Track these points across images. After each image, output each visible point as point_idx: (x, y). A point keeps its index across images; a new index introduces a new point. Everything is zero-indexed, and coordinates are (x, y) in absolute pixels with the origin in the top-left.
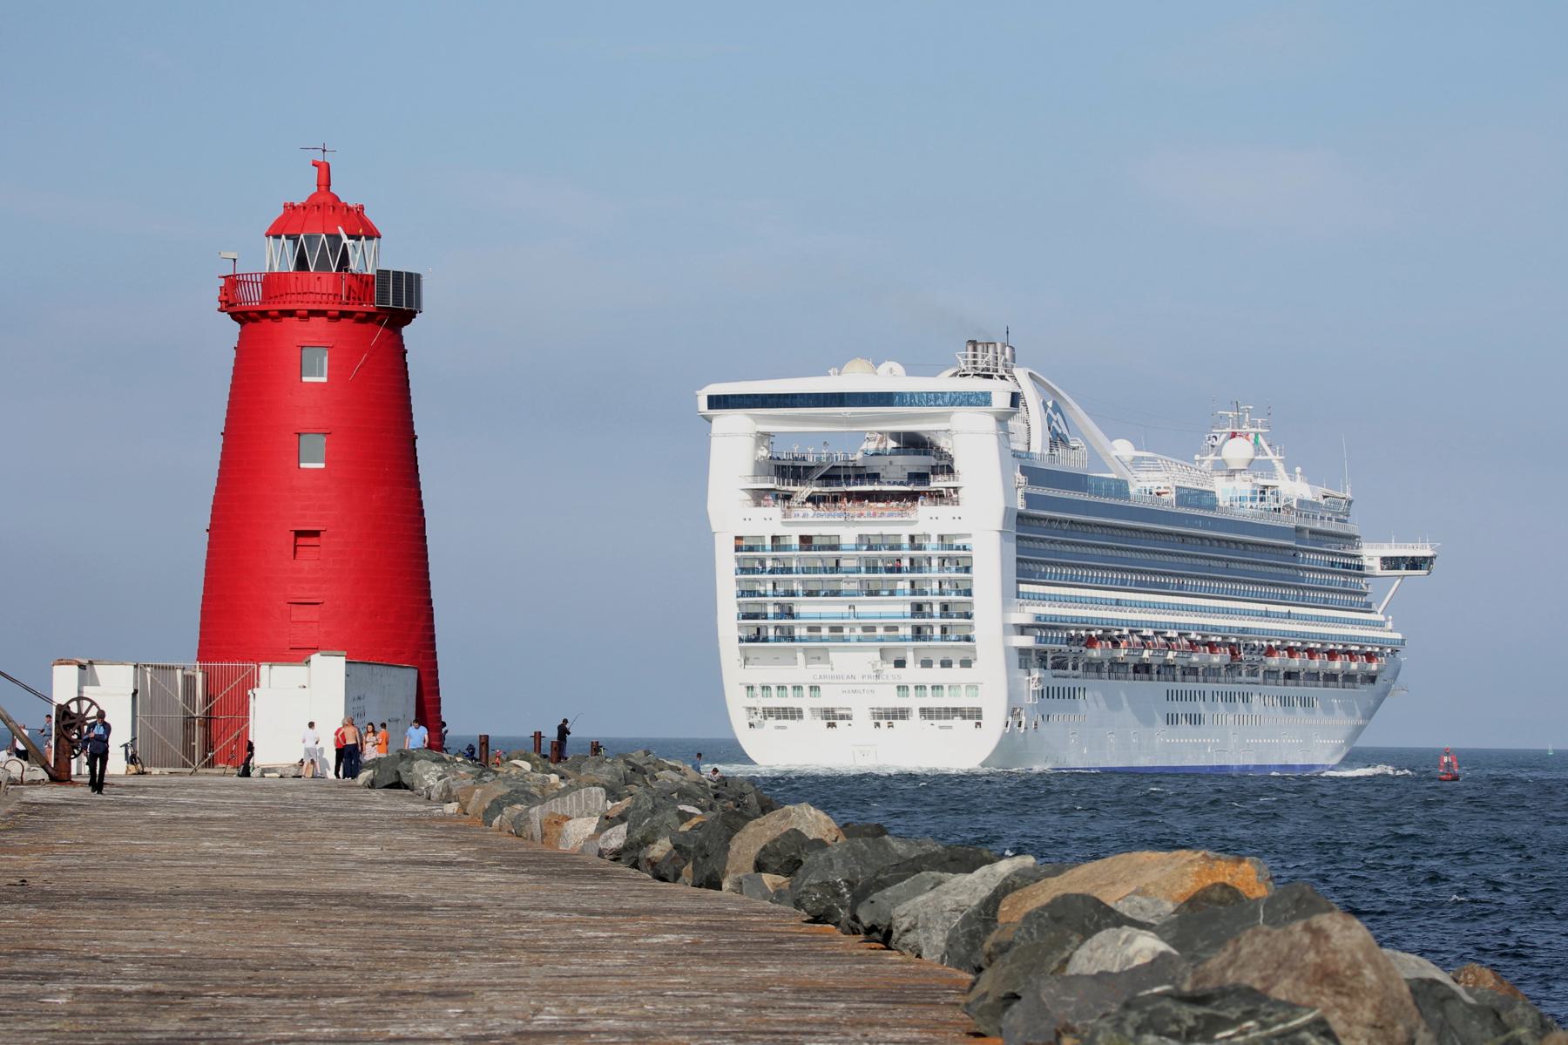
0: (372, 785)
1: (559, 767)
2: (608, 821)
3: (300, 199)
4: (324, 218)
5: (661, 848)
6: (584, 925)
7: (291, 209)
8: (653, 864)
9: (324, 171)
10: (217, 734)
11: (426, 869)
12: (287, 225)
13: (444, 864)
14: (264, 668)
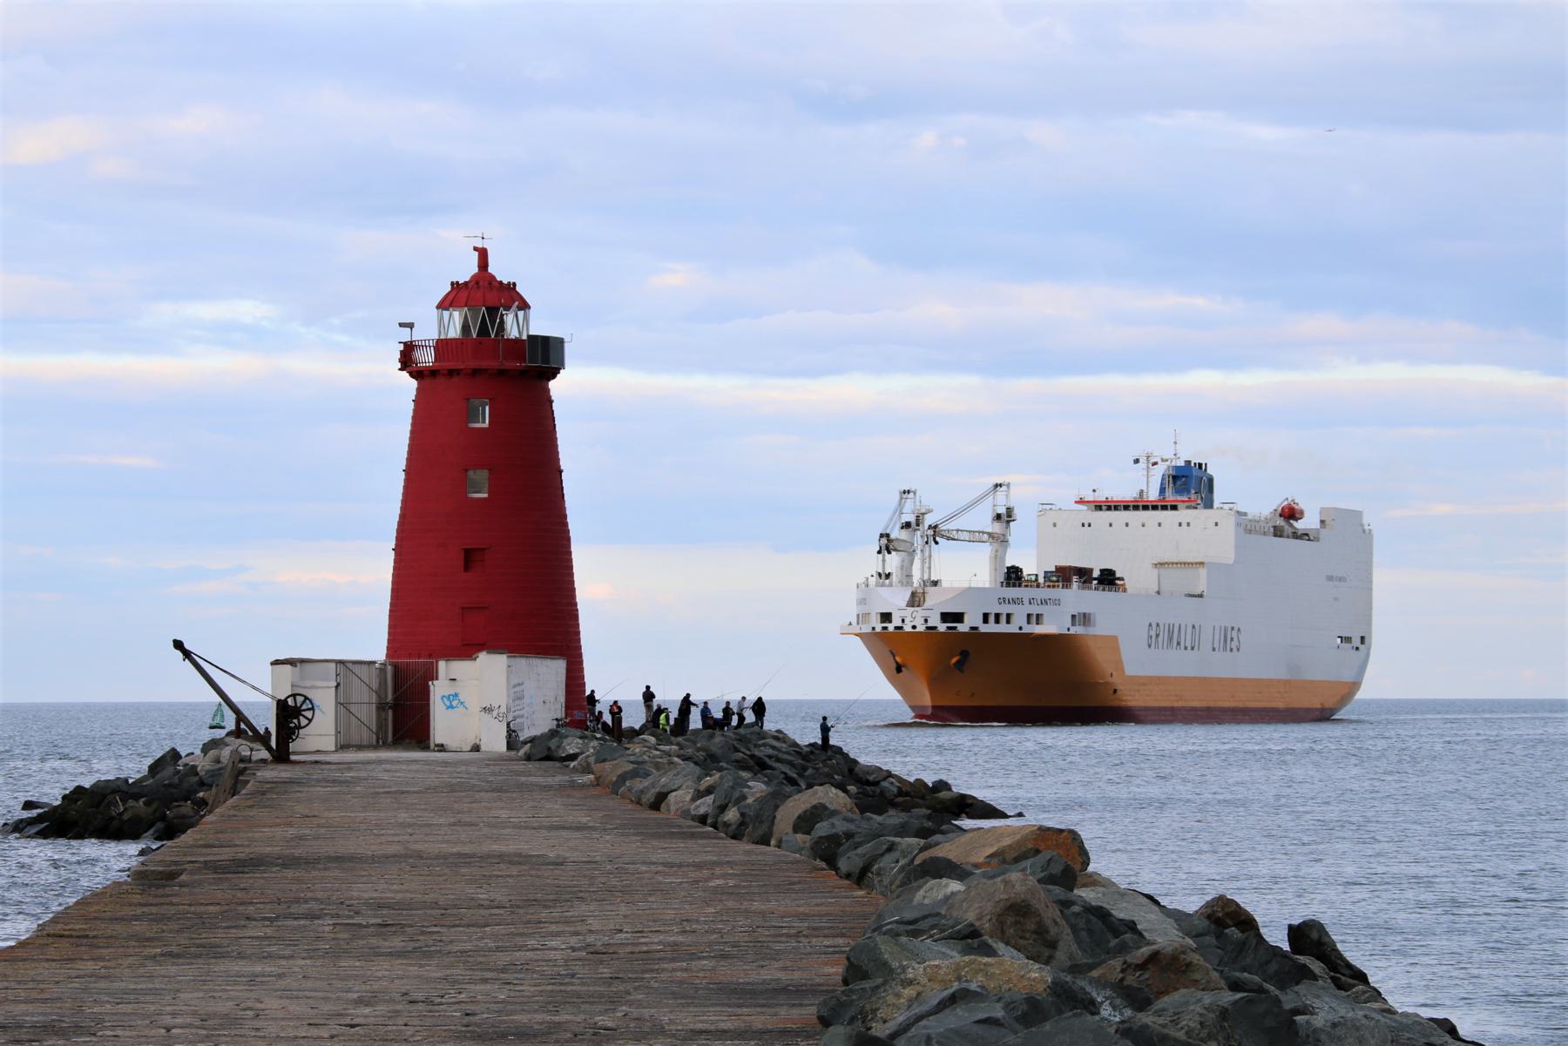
0: (528, 758)
1: (680, 739)
2: (699, 795)
3: (464, 277)
4: (485, 295)
5: (732, 815)
6: (665, 874)
7: (456, 286)
8: (727, 825)
9: (483, 254)
10: (403, 712)
11: (564, 833)
12: (457, 296)
13: (578, 829)
14: (442, 664)
